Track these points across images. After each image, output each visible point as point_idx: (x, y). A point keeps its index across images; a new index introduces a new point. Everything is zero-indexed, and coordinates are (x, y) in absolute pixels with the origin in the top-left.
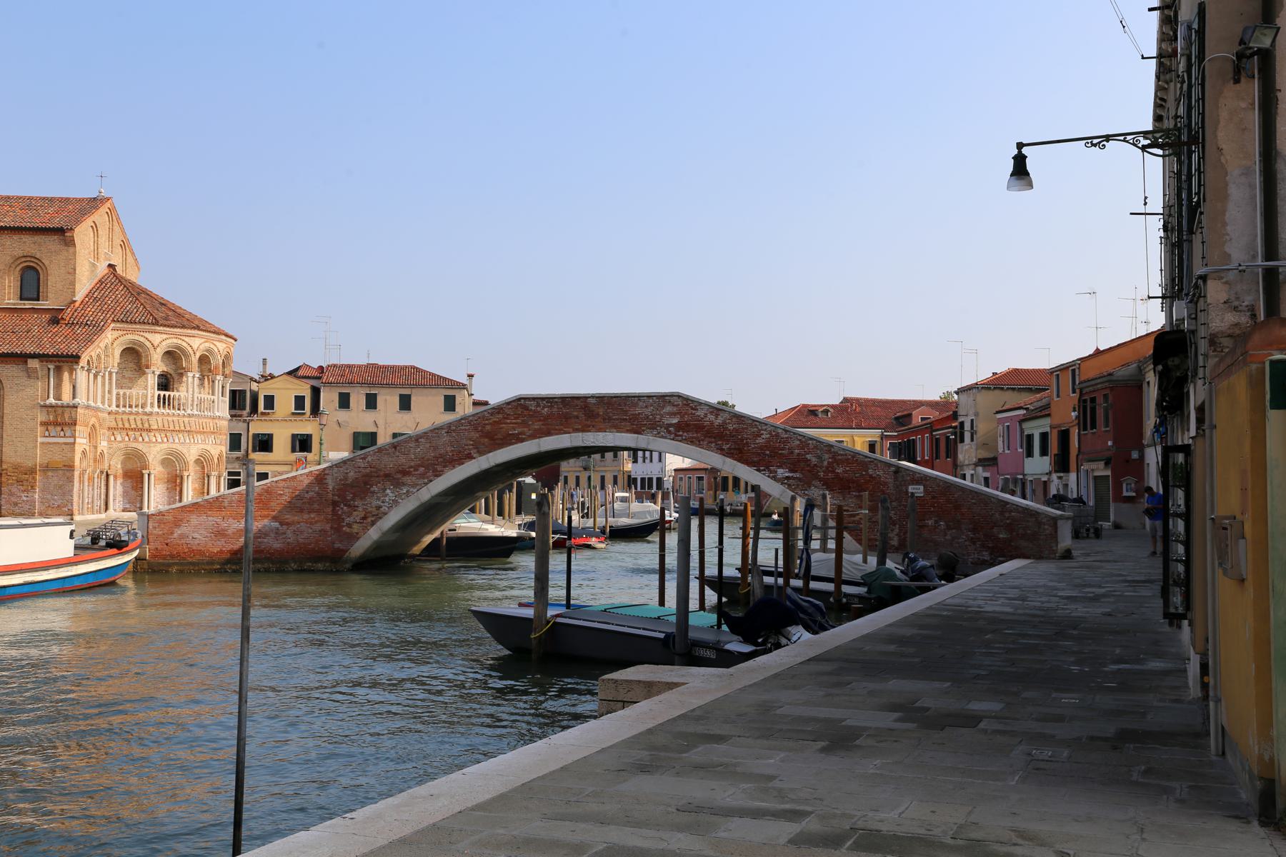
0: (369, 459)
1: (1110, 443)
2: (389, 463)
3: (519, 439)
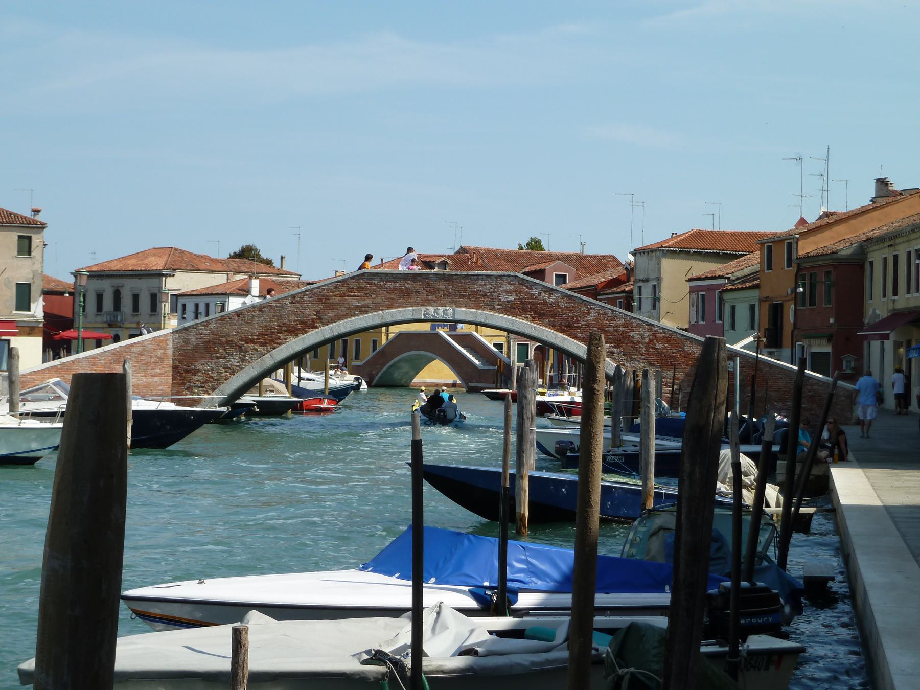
0: (212, 326)
1: (832, 321)
2: (231, 331)
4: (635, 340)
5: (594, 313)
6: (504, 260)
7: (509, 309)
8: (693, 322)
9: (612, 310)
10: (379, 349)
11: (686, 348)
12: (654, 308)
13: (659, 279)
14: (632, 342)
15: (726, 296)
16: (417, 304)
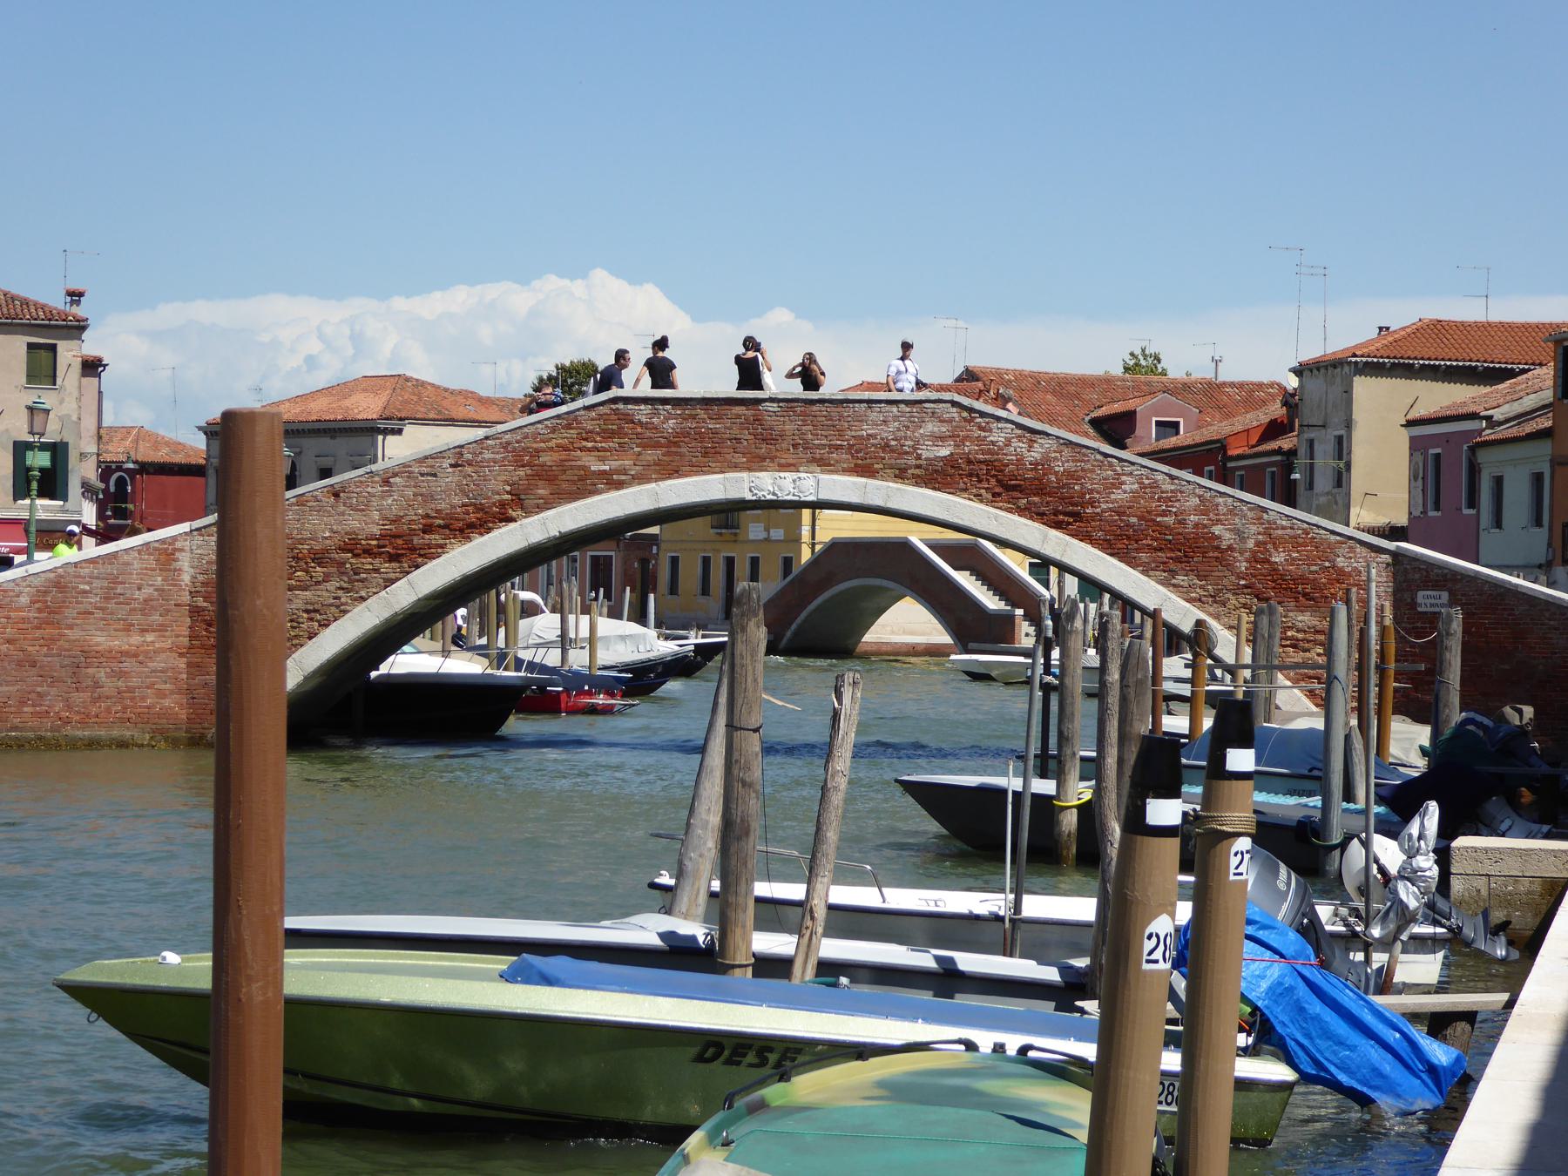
3: (613, 482)
4: (1224, 545)
5: (1130, 485)
6: (1054, 393)
7: (938, 477)
8: (1417, 513)
9: (1172, 477)
10: (795, 570)
11: (1341, 562)
12: (1339, 484)
13: (1349, 424)
14: (1218, 548)
15: (1483, 456)
16: (736, 467)
